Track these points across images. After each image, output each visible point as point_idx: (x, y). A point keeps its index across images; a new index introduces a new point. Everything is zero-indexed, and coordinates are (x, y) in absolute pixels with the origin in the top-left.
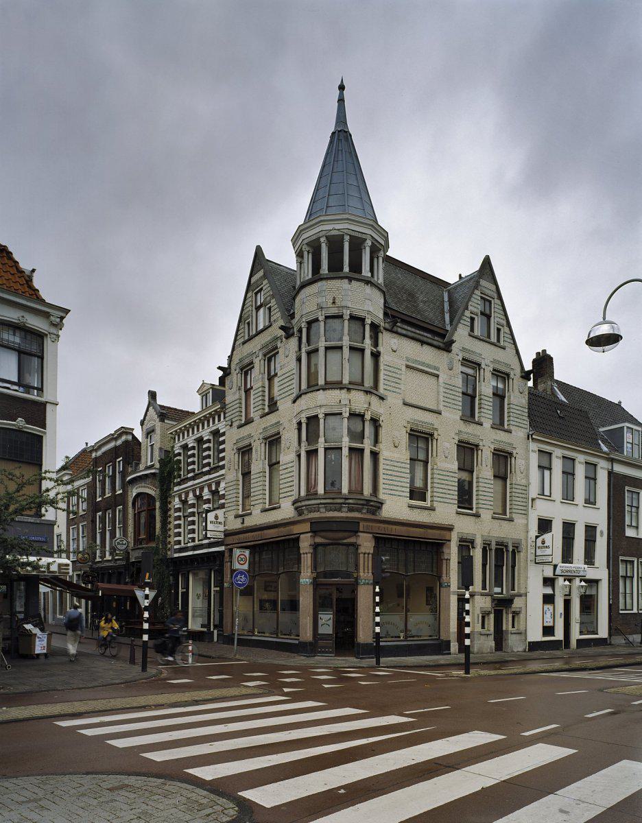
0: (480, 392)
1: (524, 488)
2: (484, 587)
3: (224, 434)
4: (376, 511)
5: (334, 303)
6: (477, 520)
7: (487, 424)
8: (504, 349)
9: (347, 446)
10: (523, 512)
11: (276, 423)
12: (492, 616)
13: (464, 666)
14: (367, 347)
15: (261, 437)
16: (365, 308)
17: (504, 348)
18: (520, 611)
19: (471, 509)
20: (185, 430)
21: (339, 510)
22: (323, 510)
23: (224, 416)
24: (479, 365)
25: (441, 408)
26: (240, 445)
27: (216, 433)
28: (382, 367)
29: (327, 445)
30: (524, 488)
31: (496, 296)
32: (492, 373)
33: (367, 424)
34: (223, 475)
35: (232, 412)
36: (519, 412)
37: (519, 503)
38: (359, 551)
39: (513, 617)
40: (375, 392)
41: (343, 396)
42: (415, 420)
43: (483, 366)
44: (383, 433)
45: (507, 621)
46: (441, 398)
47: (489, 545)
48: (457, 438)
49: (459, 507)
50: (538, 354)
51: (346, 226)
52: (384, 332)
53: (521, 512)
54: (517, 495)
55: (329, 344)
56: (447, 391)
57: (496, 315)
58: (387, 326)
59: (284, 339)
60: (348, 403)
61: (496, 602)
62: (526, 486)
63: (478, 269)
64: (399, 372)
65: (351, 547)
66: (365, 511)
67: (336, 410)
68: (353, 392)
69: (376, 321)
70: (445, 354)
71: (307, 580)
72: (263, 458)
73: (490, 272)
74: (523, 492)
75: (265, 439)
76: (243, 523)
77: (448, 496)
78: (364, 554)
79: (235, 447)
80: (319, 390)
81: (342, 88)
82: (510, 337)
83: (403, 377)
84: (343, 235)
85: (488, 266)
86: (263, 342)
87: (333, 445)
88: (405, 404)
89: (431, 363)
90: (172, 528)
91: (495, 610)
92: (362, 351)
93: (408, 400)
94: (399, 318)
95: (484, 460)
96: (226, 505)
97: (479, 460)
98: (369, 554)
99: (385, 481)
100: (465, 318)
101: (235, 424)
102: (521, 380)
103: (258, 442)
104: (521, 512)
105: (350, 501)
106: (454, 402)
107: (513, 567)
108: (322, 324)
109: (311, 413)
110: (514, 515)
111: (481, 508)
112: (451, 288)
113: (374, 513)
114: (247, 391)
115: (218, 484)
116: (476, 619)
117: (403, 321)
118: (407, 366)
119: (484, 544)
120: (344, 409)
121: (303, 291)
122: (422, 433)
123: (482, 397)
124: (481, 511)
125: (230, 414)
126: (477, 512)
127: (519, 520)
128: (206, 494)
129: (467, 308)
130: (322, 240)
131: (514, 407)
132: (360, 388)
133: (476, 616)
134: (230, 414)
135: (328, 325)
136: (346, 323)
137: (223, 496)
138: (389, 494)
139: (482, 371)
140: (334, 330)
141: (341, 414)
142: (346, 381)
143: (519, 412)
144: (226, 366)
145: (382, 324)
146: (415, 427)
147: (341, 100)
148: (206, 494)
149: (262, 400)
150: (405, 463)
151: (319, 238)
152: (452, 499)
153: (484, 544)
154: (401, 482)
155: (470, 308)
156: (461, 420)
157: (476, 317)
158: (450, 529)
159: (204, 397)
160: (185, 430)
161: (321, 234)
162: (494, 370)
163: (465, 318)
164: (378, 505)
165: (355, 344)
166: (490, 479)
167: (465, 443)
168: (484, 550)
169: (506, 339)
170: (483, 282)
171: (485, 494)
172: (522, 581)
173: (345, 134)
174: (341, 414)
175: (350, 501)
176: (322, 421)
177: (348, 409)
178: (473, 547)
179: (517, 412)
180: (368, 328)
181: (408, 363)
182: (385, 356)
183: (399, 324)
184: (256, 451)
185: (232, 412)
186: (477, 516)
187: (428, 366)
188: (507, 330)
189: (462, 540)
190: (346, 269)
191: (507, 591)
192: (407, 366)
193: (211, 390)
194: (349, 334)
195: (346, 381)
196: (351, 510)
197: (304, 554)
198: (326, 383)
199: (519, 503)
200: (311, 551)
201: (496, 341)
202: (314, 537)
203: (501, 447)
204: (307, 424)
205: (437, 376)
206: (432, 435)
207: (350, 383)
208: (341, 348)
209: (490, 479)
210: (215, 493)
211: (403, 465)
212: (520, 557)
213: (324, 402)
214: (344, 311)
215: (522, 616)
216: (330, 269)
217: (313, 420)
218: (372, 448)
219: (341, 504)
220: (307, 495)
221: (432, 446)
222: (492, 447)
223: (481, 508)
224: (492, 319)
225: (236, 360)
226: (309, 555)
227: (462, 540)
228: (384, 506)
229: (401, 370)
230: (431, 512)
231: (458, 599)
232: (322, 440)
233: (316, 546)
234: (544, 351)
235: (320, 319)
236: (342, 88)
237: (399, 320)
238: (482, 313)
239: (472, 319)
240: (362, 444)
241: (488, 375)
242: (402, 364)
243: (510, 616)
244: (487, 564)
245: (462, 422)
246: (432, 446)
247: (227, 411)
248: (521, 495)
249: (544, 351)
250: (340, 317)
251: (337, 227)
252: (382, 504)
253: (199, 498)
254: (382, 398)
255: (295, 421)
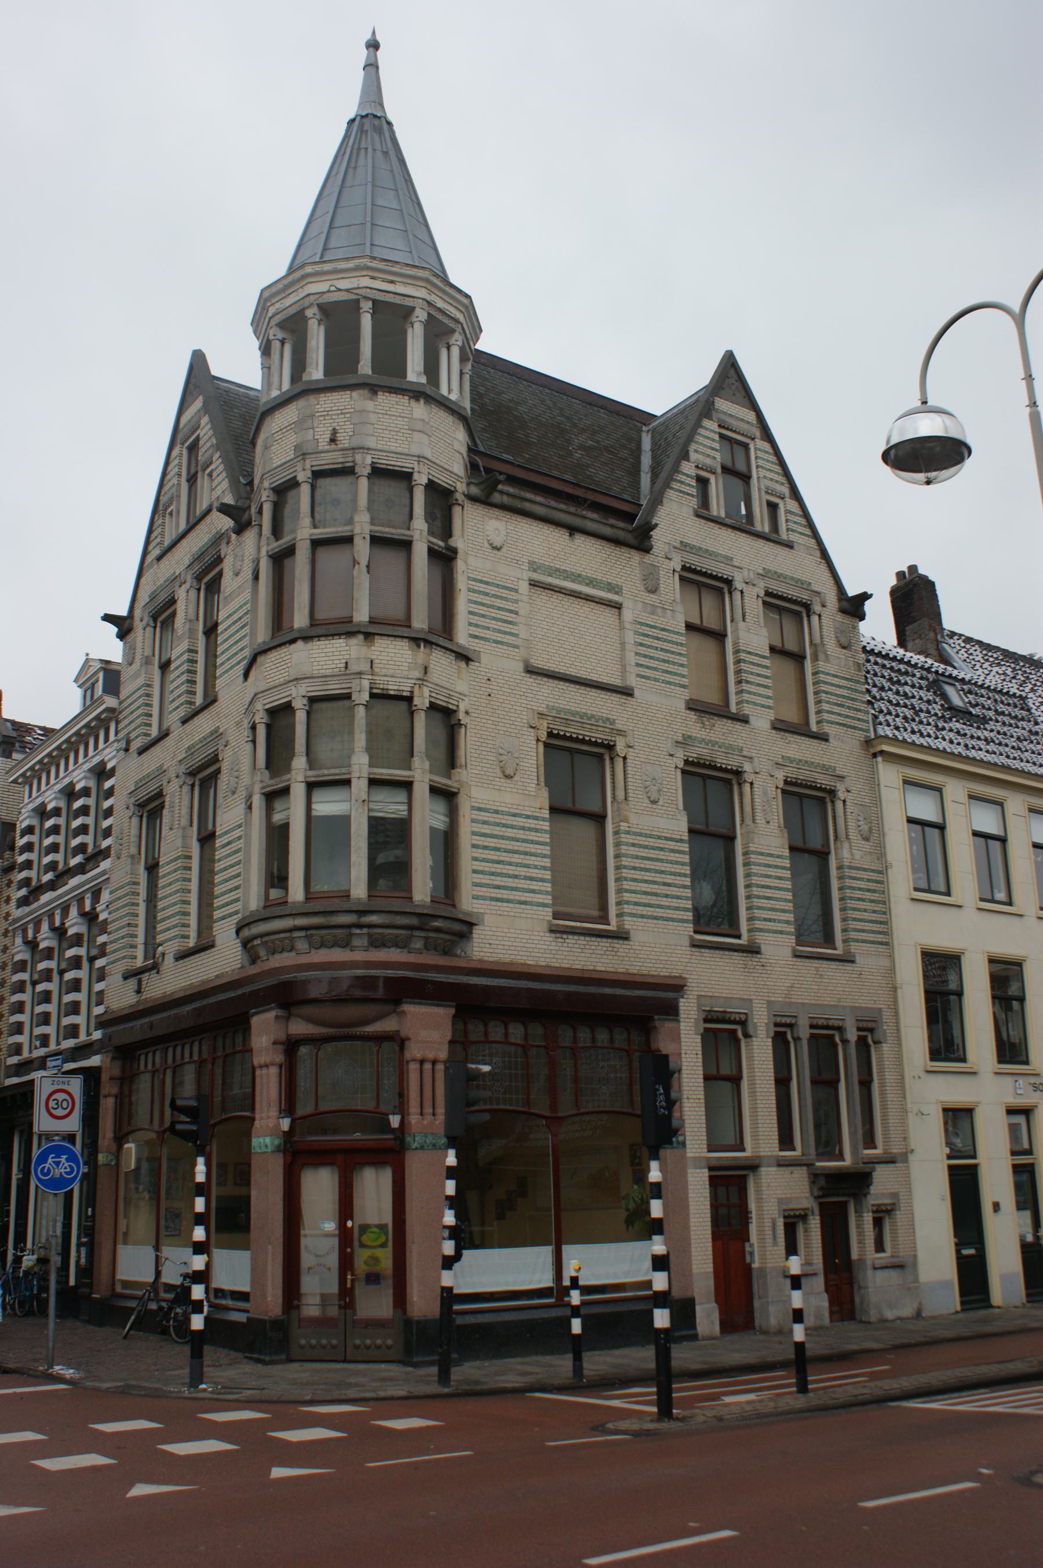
0: (736, 644)
1: (875, 876)
2: (786, 1140)
3: (113, 771)
4: (453, 943)
5: (333, 440)
6: (753, 961)
7: (761, 721)
8: (792, 547)
9: (365, 774)
10: (880, 938)
11: (212, 733)
12: (815, 1223)
13: (793, 1369)
14: (416, 535)
15: (183, 769)
16: (415, 450)
17: (789, 545)
18: (894, 1204)
19: (739, 937)
20: (42, 770)
21: (346, 944)
22: (302, 945)
23: (117, 727)
24: (729, 582)
25: (632, 681)
26: (143, 794)
27: (101, 772)
28: (462, 583)
29: (313, 775)
30: (875, 876)
31: (757, 433)
32: (765, 603)
33: (420, 721)
34: (104, 873)
35: (131, 718)
36: (844, 692)
37: (866, 916)
38: (408, 1055)
39: (878, 1223)
40: (441, 641)
41: (354, 654)
42: (559, 711)
43: (738, 584)
44: (469, 743)
45: (861, 1234)
46: (631, 658)
47: (791, 1026)
48: (680, 755)
49: (696, 932)
50: (900, 575)
51: (366, 282)
52: (468, 504)
53: (871, 937)
54: (858, 894)
55: (321, 532)
56: (647, 641)
57: (762, 473)
58: (475, 490)
59: (234, 536)
60: (365, 667)
61: (822, 1182)
62: (880, 872)
63: (706, 381)
64: (514, 596)
65: (385, 1045)
66: (418, 944)
67: (335, 687)
68: (380, 643)
69: (443, 480)
70: (636, 556)
71: (268, 1140)
72: (184, 822)
73: (738, 384)
74: (872, 886)
75: (192, 774)
76: (139, 991)
77: (665, 902)
78: (422, 1062)
79: (133, 800)
80: (293, 641)
81: (373, 45)
82: (803, 521)
83: (523, 608)
84: (358, 301)
85: (732, 372)
86: (195, 549)
87: (327, 774)
88: (531, 671)
89: (599, 576)
90: (6, 1013)
91: (822, 1206)
92: (406, 545)
93: (540, 662)
94: (501, 473)
95: (758, 808)
96: (109, 949)
97: (748, 808)
98: (434, 1062)
99: (479, 866)
100: (683, 478)
101: (135, 745)
102: (840, 617)
103: (175, 784)
104: (871, 937)
105: (374, 919)
106: (665, 666)
107: (866, 1084)
108: (305, 490)
109: (277, 699)
110: (854, 947)
111: (761, 930)
112: (658, 426)
113: (447, 951)
114: (165, 666)
115: (96, 894)
116: (769, 1233)
117: (512, 480)
118: (534, 584)
119: (776, 1025)
120: (355, 685)
121: (268, 421)
122: (583, 741)
123: (743, 656)
124: (761, 939)
125: (126, 722)
126: (751, 941)
127: (868, 959)
128: (75, 925)
129: (685, 456)
130: (309, 313)
131: (830, 679)
132: (405, 632)
133: (768, 1224)
134: (126, 722)
135: (319, 492)
136: (363, 484)
137: (104, 928)
138: (492, 899)
139: (737, 596)
140: (336, 502)
141: (348, 697)
142: (362, 615)
143: (844, 692)
144: (123, 612)
145: (461, 487)
146: (560, 728)
147: (372, 67)
148: (75, 925)
149: (188, 681)
150: (536, 818)
151: (303, 310)
152: (677, 909)
153: (776, 1025)
154: (527, 866)
155: (693, 456)
156: (689, 709)
157: (712, 479)
158: (678, 987)
159: (89, 693)
160: (42, 770)
161: (307, 302)
162: (768, 594)
163: (683, 478)
164: (457, 927)
165: (387, 530)
166: (778, 857)
167: (704, 766)
168: (781, 1041)
169: (791, 525)
170: (721, 404)
171: (768, 893)
172: (893, 1120)
173: (376, 122)
174: (348, 697)
175: (374, 919)
176: (301, 717)
177: (366, 684)
178: (747, 1036)
179: (839, 691)
180: (419, 497)
181: (536, 576)
182: (471, 560)
183: (500, 487)
184: (172, 807)
185: (131, 718)
186: (752, 950)
187: (591, 582)
188: (793, 505)
189: (710, 1017)
190: (365, 367)
191: (855, 1151)
192: (534, 584)
193: (101, 675)
194: (369, 509)
195: (362, 615)
196: (377, 943)
197: (261, 1067)
198: (313, 622)
199: (866, 916)
200: (280, 1058)
201: (767, 529)
202: (288, 1019)
203: (803, 775)
204: (269, 727)
205: (618, 607)
206: (610, 747)
207: (372, 621)
208: (348, 540)
209: (778, 857)
210: (90, 917)
211: (531, 823)
212: (882, 1056)
213: (306, 670)
214: (358, 458)
215: (899, 1216)
216: (329, 370)
217: (281, 713)
218: (437, 778)
219: (350, 926)
220: (265, 907)
221: (613, 775)
222: (780, 775)
223: (761, 930)
224: (754, 481)
225: (144, 597)
226: (274, 1071)
227: (710, 1017)
228: (477, 932)
229: (516, 591)
230: (617, 944)
231: (711, 1178)
232: (299, 763)
233: (291, 1046)
234: (913, 569)
235: (301, 477)
236: (373, 45)
237: (502, 477)
238: (726, 470)
239: (703, 483)
240: (410, 769)
241: (754, 606)
242: (519, 577)
243: (868, 1218)
244: (838, 1081)
245: (692, 716)
246: (613, 775)
247: (121, 717)
248: (868, 895)
249: (913, 569)
250: (347, 471)
251: (344, 284)
252: (471, 925)
253: (60, 932)
254: (464, 657)
255: (246, 724)
